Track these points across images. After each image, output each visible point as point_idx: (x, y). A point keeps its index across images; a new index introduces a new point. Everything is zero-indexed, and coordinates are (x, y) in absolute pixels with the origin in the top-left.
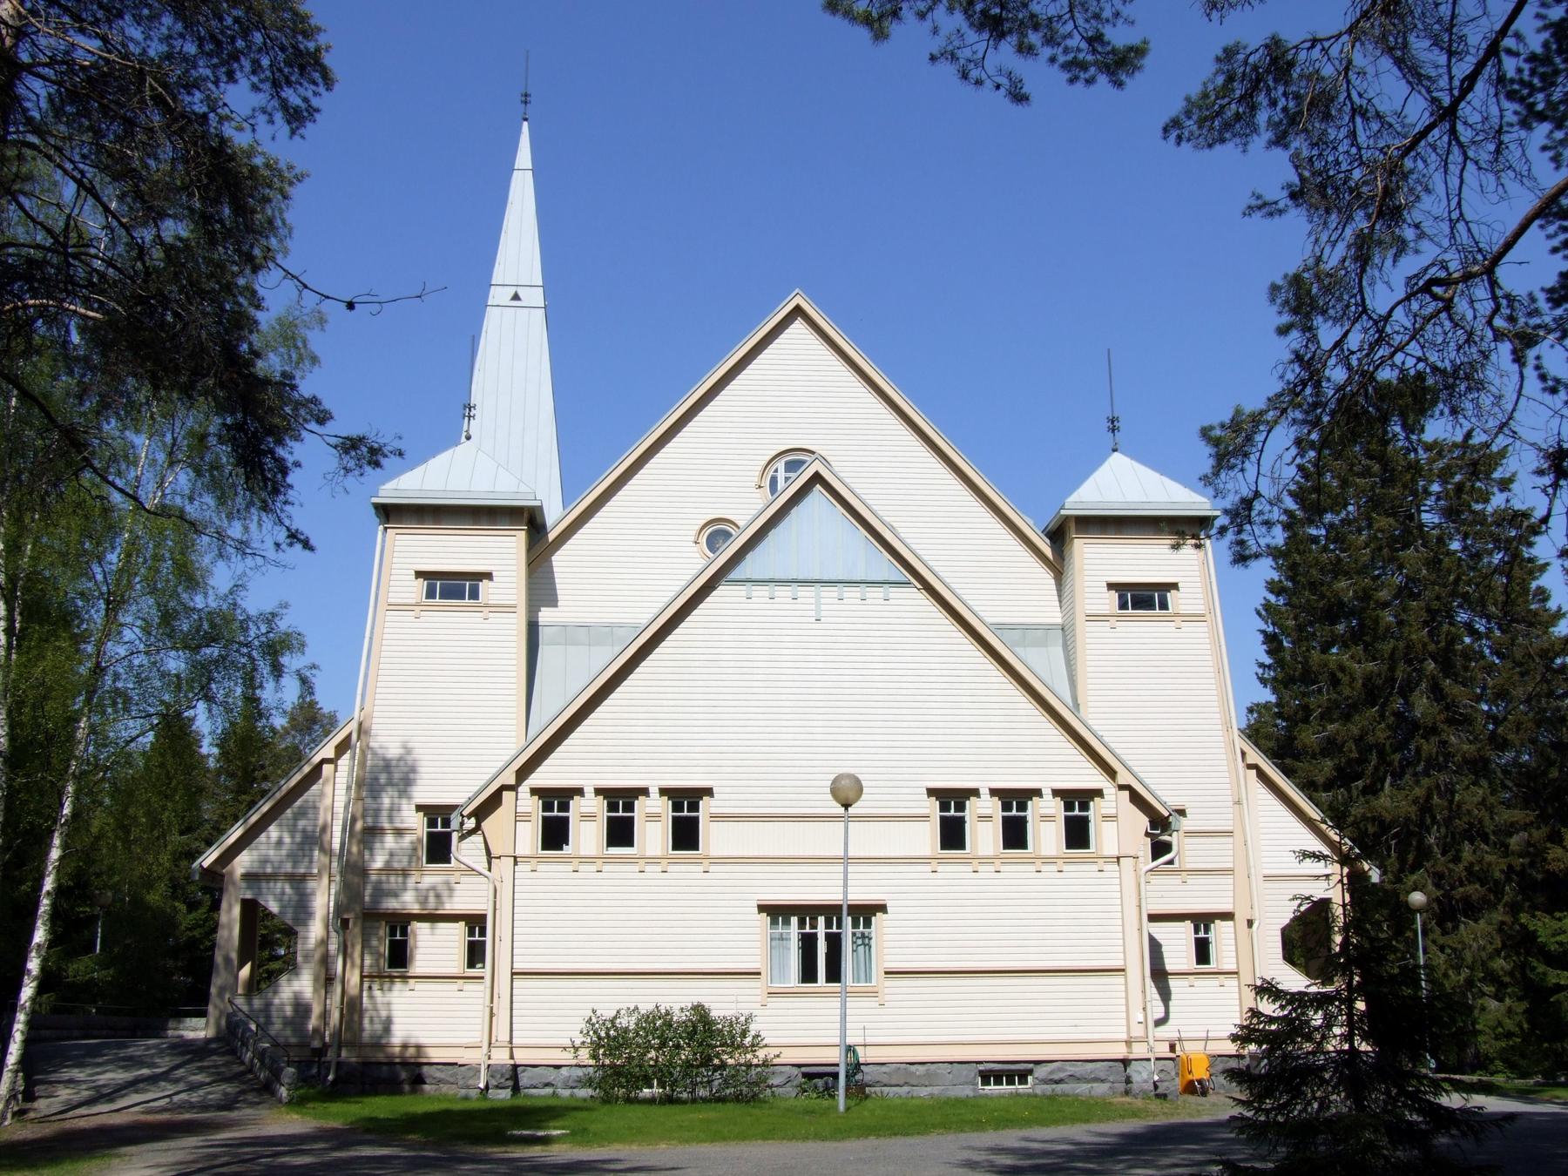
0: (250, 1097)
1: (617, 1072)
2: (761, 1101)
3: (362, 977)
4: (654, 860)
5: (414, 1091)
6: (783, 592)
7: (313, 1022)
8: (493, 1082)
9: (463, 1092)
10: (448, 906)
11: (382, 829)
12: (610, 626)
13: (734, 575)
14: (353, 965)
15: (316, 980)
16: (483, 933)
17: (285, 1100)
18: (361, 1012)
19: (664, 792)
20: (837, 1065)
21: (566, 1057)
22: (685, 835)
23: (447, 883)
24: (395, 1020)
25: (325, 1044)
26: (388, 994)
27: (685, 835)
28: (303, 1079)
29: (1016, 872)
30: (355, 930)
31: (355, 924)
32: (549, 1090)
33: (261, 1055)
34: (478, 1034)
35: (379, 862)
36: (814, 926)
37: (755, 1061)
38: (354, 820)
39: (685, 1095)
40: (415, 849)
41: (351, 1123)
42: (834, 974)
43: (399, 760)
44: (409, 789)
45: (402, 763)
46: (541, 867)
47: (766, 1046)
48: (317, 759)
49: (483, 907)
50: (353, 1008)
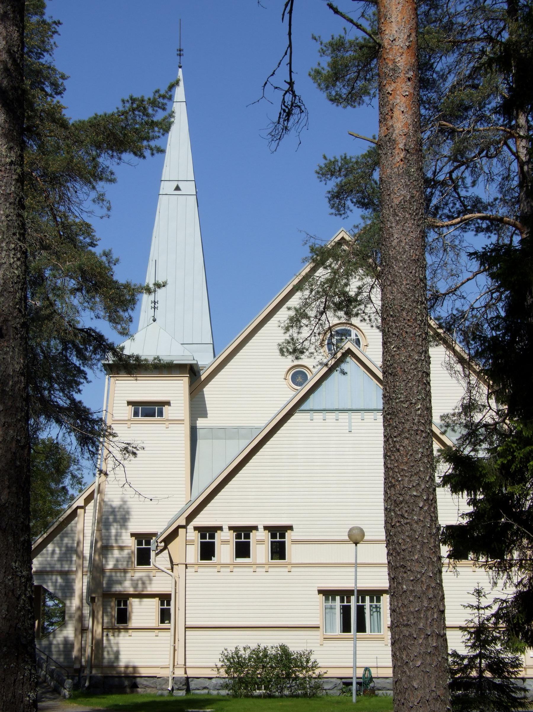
0: (48, 695)
1: (241, 681)
2: (317, 697)
3: (103, 629)
4: (261, 565)
5: (132, 692)
6: (331, 416)
7: (75, 653)
8: (176, 687)
9: (160, 692)
10: (149, 589)
11: (112, 547)
12: (238, 428)
13: (303, 407)
14: (98, 622)
15: (76, 630)
16: (169, 604)
17: (67, 697)
18: (103, 649)
19: (266, 528)
20: (352, 678)
21: (213, 673)
23: (149, 576)
24: (122, 653)
25: (82, 666)
26: (117, 638)
28: (76, 687)
30: (98, 602)
31: (98, 600)
32: (206, 691)
33: (51, 673)
34: (167, 661)
35: (110, 565)
36: (349, 601)
37: (314, 676)
38: (96, 542)
39: (277, 694)
40: (130, 558)
41: (107, 707)
42: (361, 628)
43: (120, 508)
44: (126, 524)
45: (121, 510)
46: (200, 570)
47: (319, 667)
48: (74, 506)
49: (170, 589)
50: (98, 646)
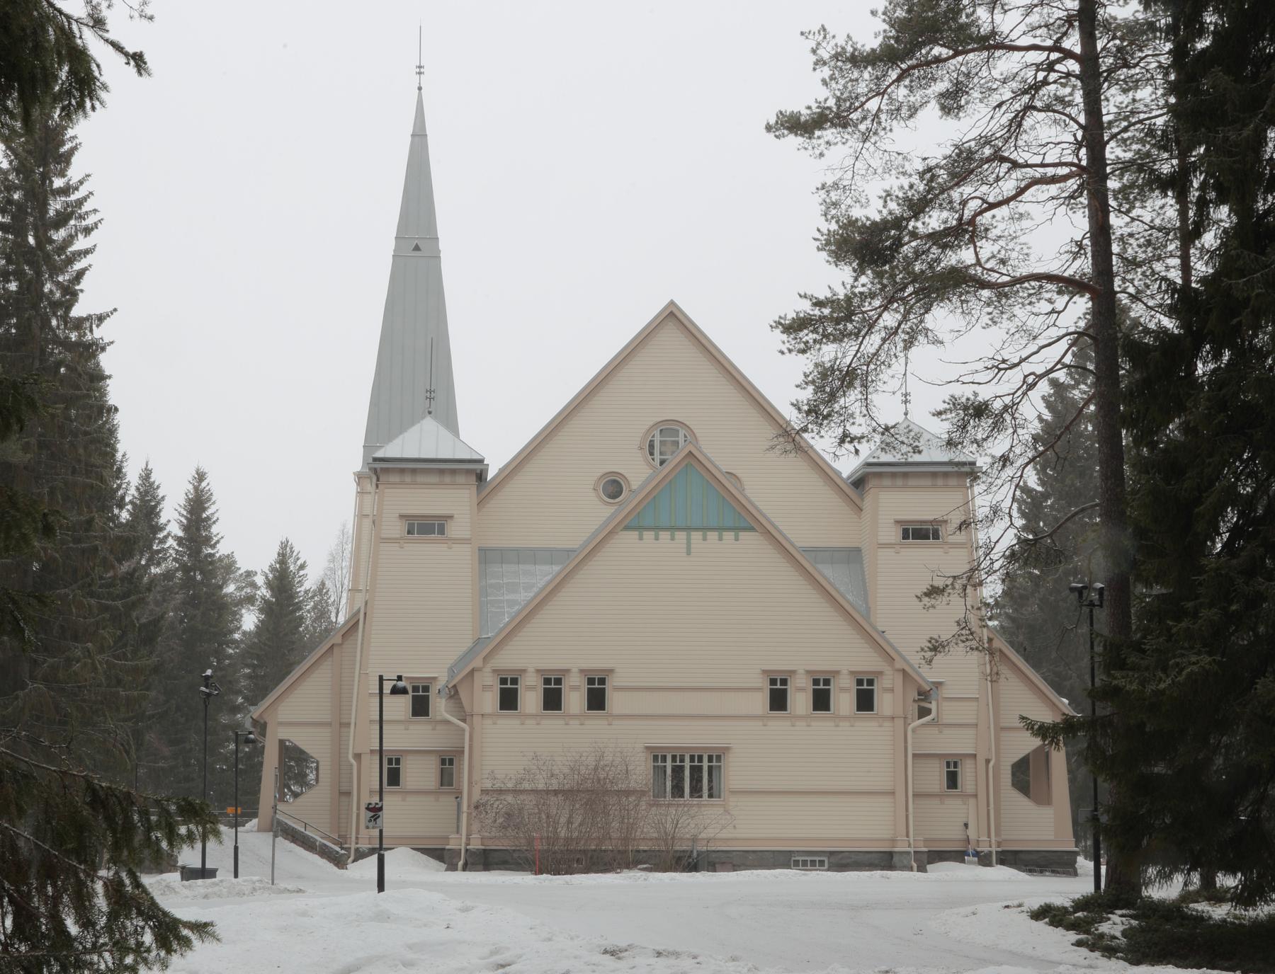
22: (596, 700)
27: (596, 700)
29: (822, 725)
